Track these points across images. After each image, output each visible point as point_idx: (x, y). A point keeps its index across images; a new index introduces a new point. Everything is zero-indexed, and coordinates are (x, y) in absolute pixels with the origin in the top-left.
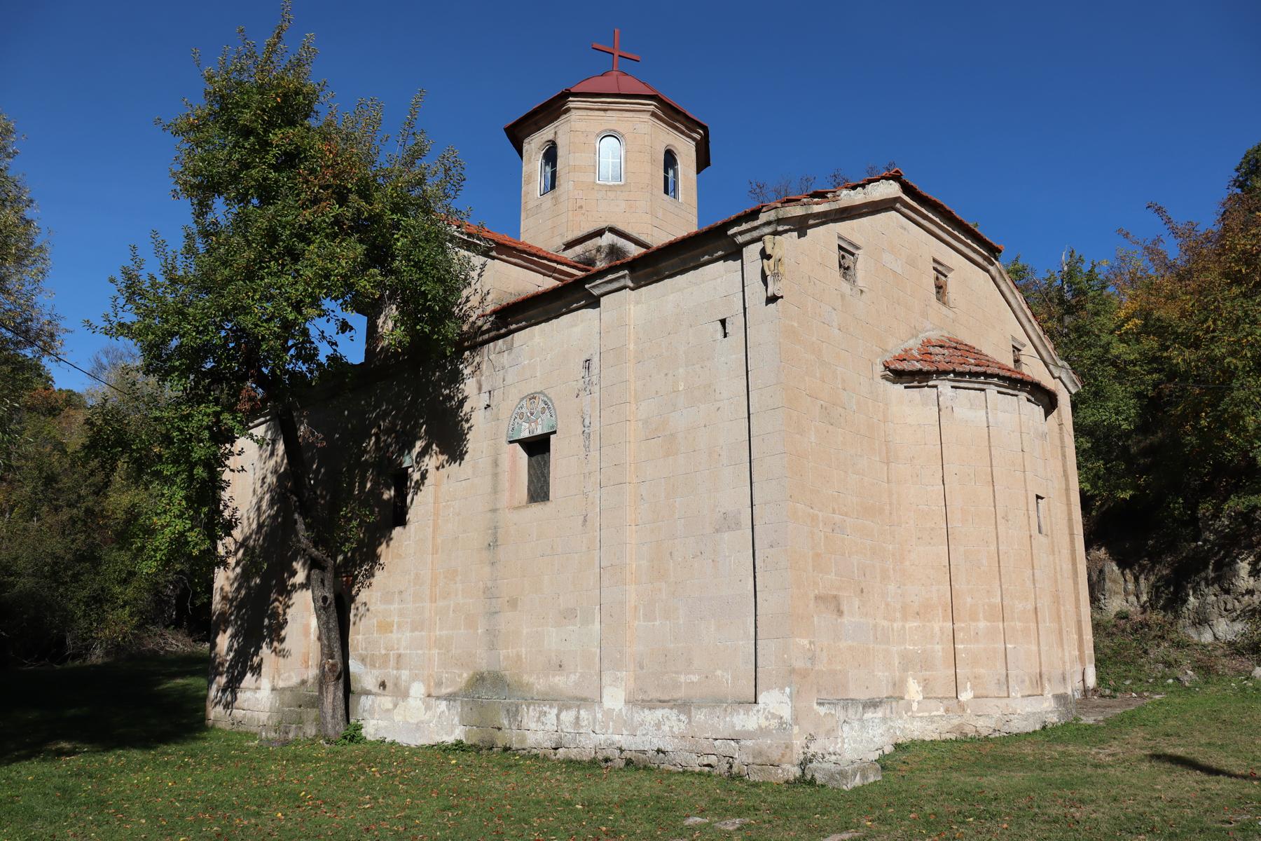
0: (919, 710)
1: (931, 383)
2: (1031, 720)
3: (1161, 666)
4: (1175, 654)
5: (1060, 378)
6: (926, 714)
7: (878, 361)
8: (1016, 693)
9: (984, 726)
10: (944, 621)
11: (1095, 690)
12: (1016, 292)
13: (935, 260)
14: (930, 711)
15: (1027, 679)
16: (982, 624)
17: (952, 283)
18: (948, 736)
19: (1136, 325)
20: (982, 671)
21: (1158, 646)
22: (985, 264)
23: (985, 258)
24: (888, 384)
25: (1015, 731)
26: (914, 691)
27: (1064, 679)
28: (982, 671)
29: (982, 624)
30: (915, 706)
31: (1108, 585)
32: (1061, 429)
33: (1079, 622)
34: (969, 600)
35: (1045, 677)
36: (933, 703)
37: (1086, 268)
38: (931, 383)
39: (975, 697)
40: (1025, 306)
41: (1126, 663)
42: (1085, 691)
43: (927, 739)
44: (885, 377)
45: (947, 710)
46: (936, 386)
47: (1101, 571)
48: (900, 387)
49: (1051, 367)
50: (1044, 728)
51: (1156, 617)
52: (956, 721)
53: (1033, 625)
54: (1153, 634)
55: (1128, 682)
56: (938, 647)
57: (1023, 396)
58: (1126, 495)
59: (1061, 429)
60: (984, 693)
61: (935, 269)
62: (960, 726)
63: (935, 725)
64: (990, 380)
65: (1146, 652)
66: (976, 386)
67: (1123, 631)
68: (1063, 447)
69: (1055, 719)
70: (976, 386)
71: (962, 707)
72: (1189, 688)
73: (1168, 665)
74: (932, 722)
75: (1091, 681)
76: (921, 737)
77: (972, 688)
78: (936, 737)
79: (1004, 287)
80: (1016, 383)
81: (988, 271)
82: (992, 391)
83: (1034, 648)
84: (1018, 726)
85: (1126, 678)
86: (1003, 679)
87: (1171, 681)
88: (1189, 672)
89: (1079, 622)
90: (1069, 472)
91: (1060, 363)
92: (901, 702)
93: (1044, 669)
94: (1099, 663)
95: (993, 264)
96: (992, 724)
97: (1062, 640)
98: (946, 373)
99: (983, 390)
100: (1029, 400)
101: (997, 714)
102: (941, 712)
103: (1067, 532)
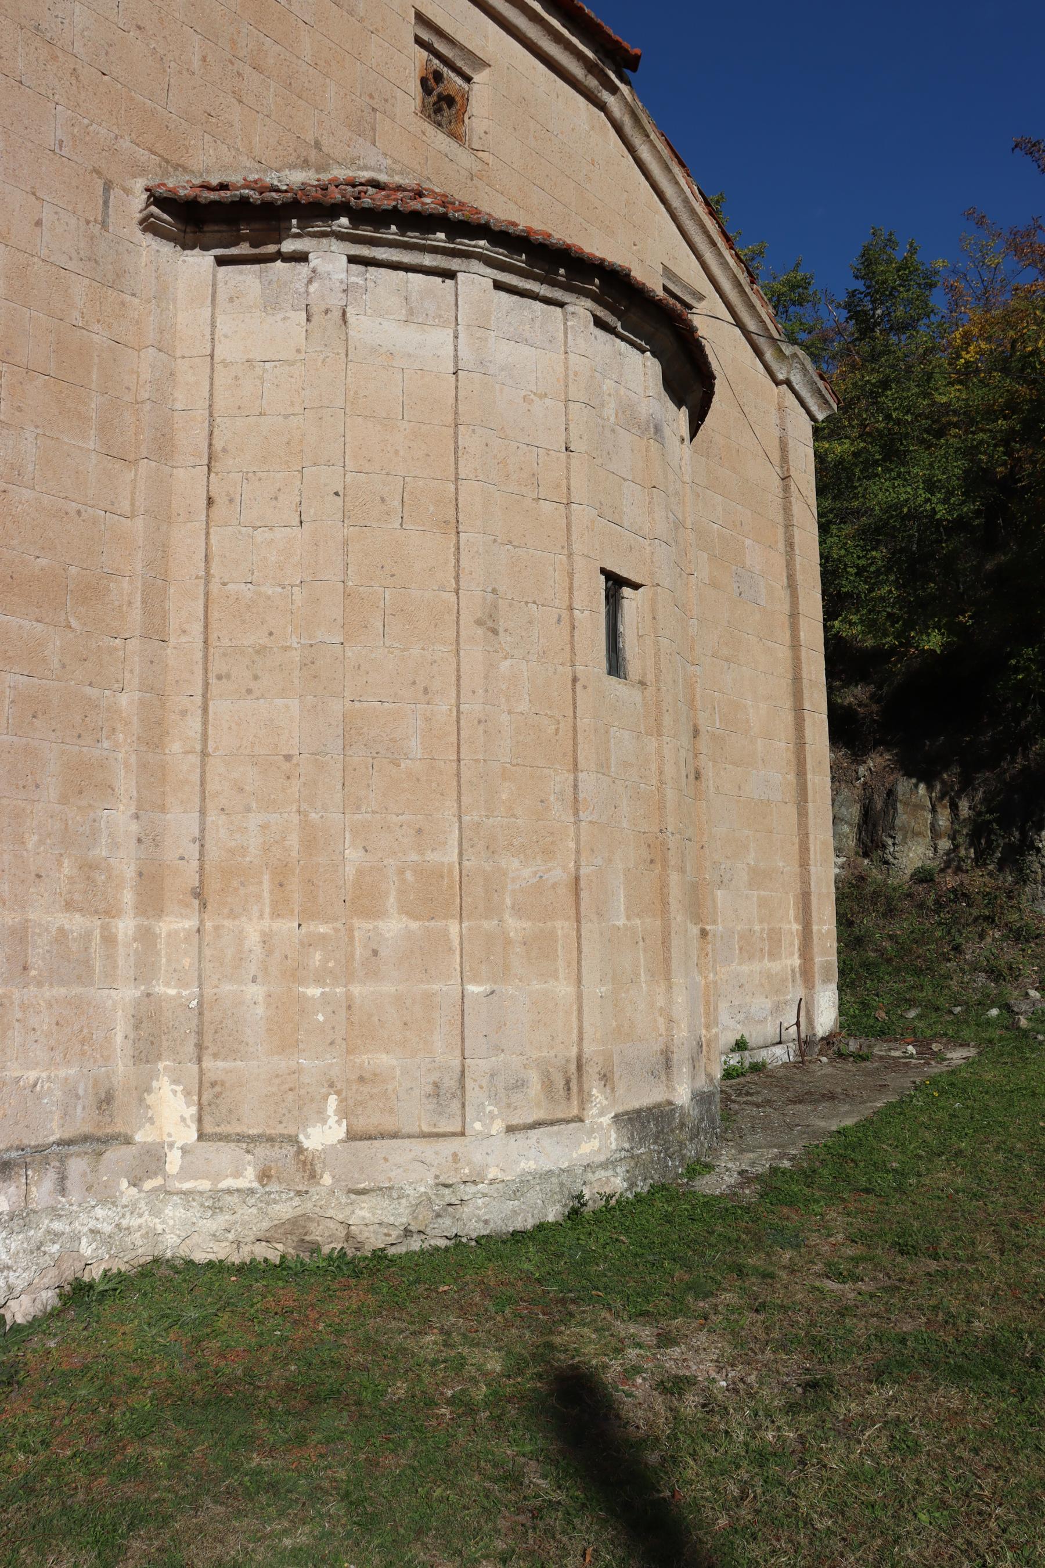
0: (185, 1173)
1: (288, 246)
2: (534, 1197)
3: (982, 978)
4: (1011, 954)
5: (788, 383)
6: (205, 1185)
7: (139, 185)
8: (487, 1121)
9: (372, 1223)
10: (276, 915)
11: (828, 1040)
12: (677, 170)
13: (421, 19)
14: (217, 1177)
15: (534, 1078)
16: (394, 926)
17: (482, 95)
18: (262, 1251)
19: (981, 352)
20: (385, 1060)
21: (982, 936)
22: (592, 82)
23: (591, 68)
24: (167, 249)
25: (475, 1229)
26: (170, 1114)
27: (668, 1065)
28: (385, 1060)
29: (394, 926)
30: (174, 1161)
31: (902, 817)
32: (786, 489)
33: (805, 898)
34: (353, 855)
35: (592, 1072)
36: (225, 1155)
37: (900, 253)
38: (288, 246)
39: (352, 1136)
40: (700, 209)
41: (919, 972)
42: (805, 1044)
43: (200, 1257)
44: (148, 226)
45: (264, 1176)
46: (301, 258)
47: (891, 793)
48: (200, 262)
49: (769, 355)
50: (574, 1214)
51: (978, 881)
52: (285, 1210)
53: (563, 927)
54: (975, 912)
55: (912, 1014)
56: (255, 992)
57: (582, 308)
58: (934, 641)
59: (786, 489)
60: (389, 1123)
61: (418, 41)
62: (296, 1225)
63: (222, 1220)
64: (465, 244)
65: (957, 949)
66: (428, 260)
67: (921, 906)
68: (788, 526)
69: (617, 1183)
70: (428, 260)
71: (308, 1166)
72: (1025, 1033)
73: (995, 974)
74: (216, 1210)
75: (826, 1017)
76: (184, 1252)
77: (344, 1112)
78: (220, 1251)
79: (645, 153)
80: (547, 264)
81: (602, 107)
82: (476, 281)
83: (564, 989)
84: (485, 1214)
85: (911, 1003)
86: (450, 1083)
87: (994, 1012)
88: (1032, 993)
89: (805, 898)
90: (800, 578)
91: (788, 349)
92: (114, 1154)
93: (589, 1049)
94: (850, 977)
95: (614, 90)
96: (398, 1214)
97: (667, 961)
98: (333, 211)
99: (449, 275)
100: (599, 323)
101: (418, 1183)
102: (248, 1179)
103: (789, 704)
